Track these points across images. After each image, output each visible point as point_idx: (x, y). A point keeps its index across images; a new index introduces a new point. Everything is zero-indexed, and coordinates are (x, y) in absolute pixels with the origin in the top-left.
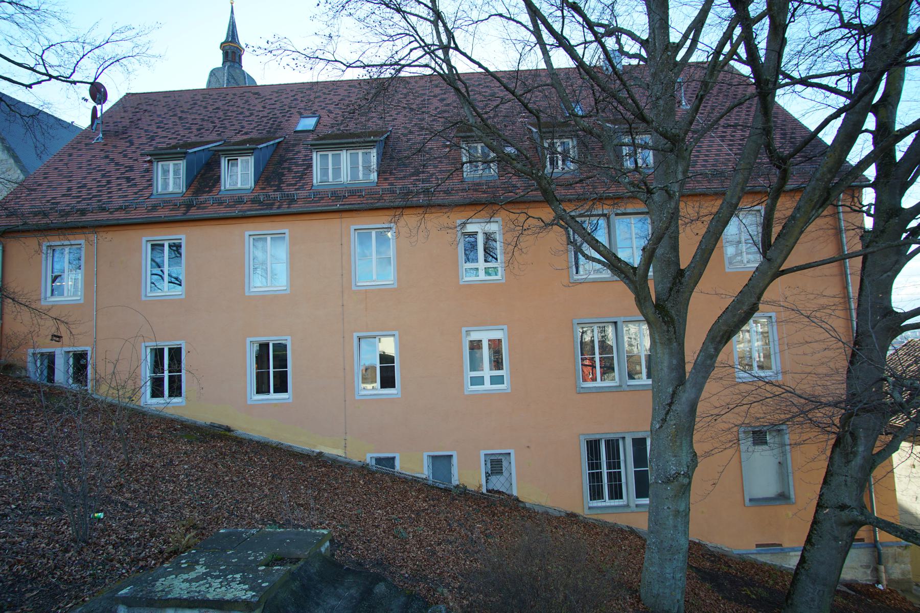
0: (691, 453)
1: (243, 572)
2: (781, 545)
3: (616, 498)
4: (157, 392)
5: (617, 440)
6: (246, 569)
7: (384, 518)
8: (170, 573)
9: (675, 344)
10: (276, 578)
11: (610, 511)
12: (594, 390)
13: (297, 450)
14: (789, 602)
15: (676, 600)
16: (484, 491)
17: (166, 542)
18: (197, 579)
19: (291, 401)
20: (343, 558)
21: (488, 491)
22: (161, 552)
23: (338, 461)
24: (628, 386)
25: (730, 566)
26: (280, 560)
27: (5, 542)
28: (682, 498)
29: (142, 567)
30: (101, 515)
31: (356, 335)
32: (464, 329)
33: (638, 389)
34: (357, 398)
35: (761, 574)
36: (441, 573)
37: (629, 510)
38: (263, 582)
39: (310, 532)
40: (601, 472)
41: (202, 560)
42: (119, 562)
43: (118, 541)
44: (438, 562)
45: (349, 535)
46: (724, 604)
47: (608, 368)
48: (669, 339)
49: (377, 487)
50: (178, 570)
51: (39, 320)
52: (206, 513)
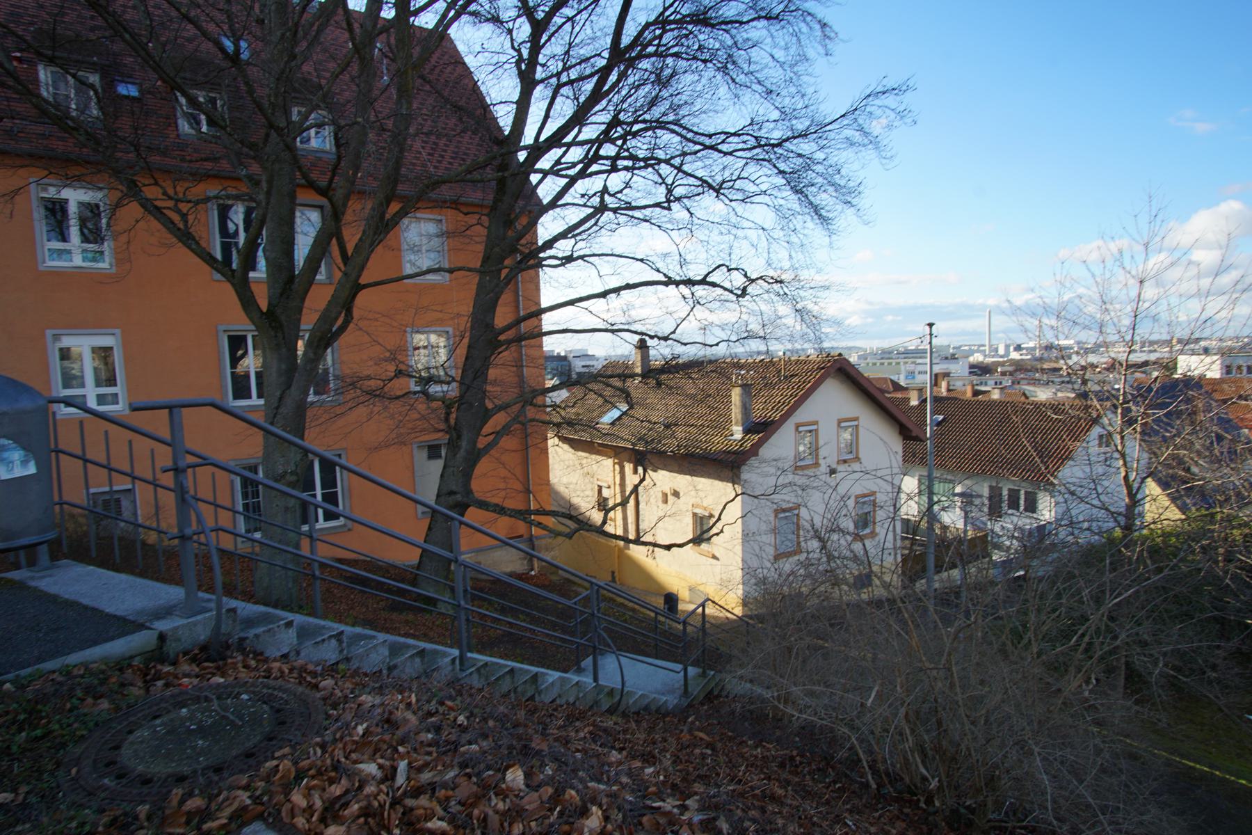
9: (284, 350)
32: (49, 333)
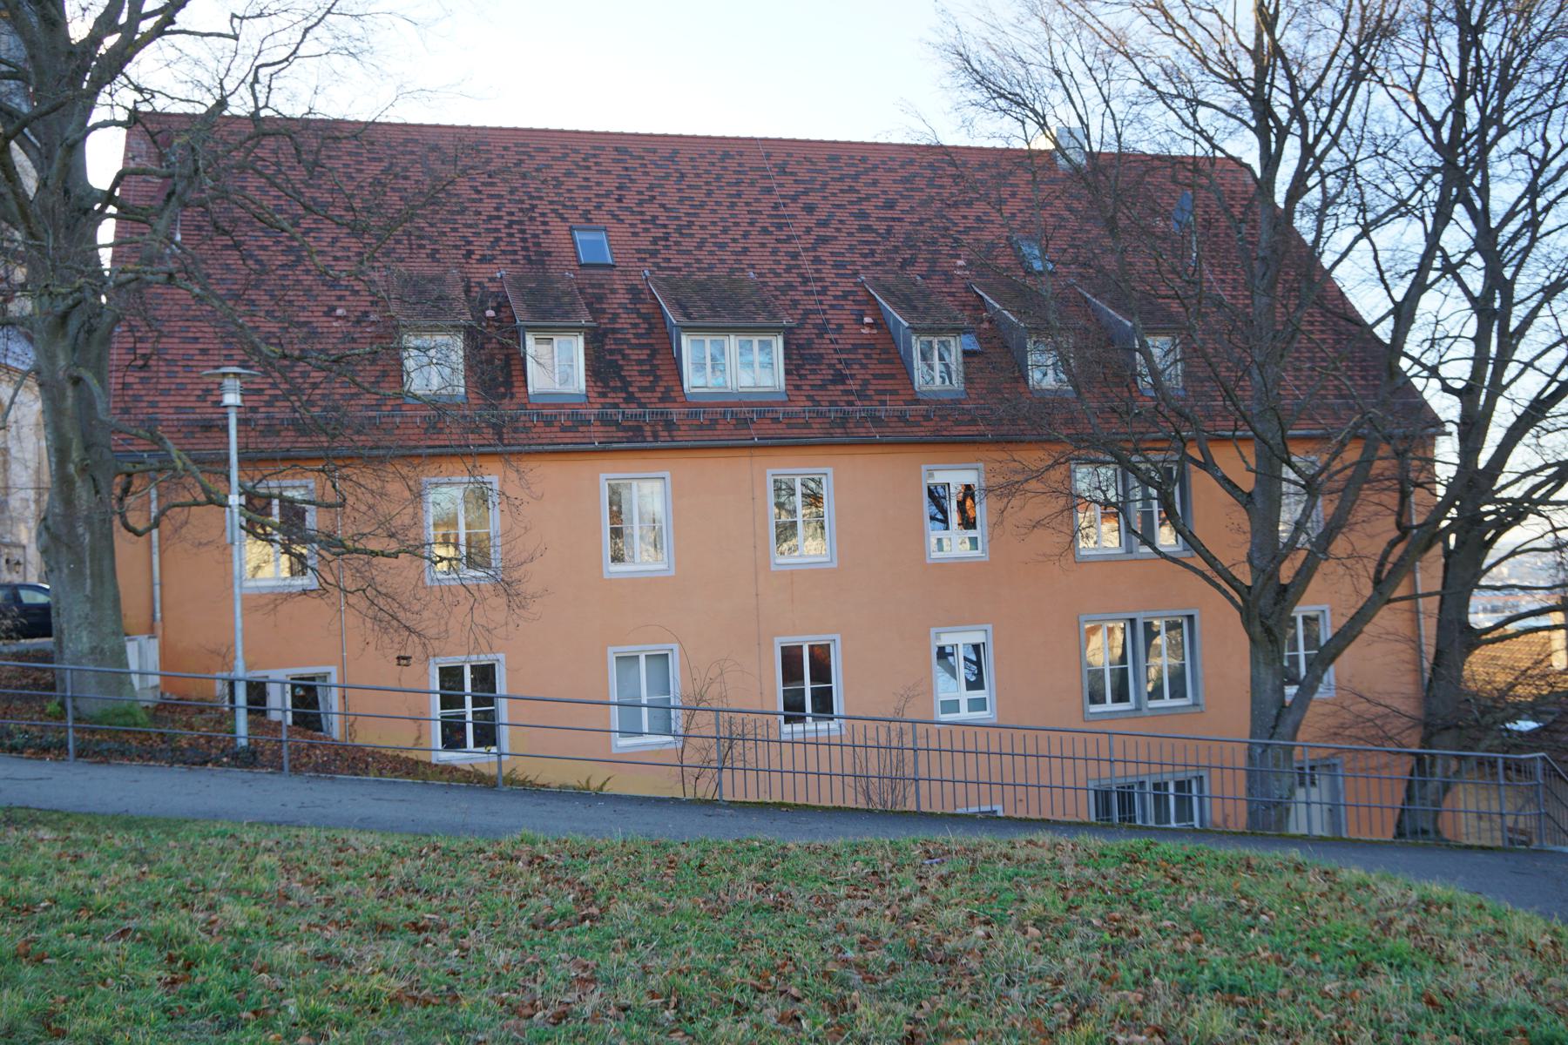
12: (1165, 712)
32: (933, 630)
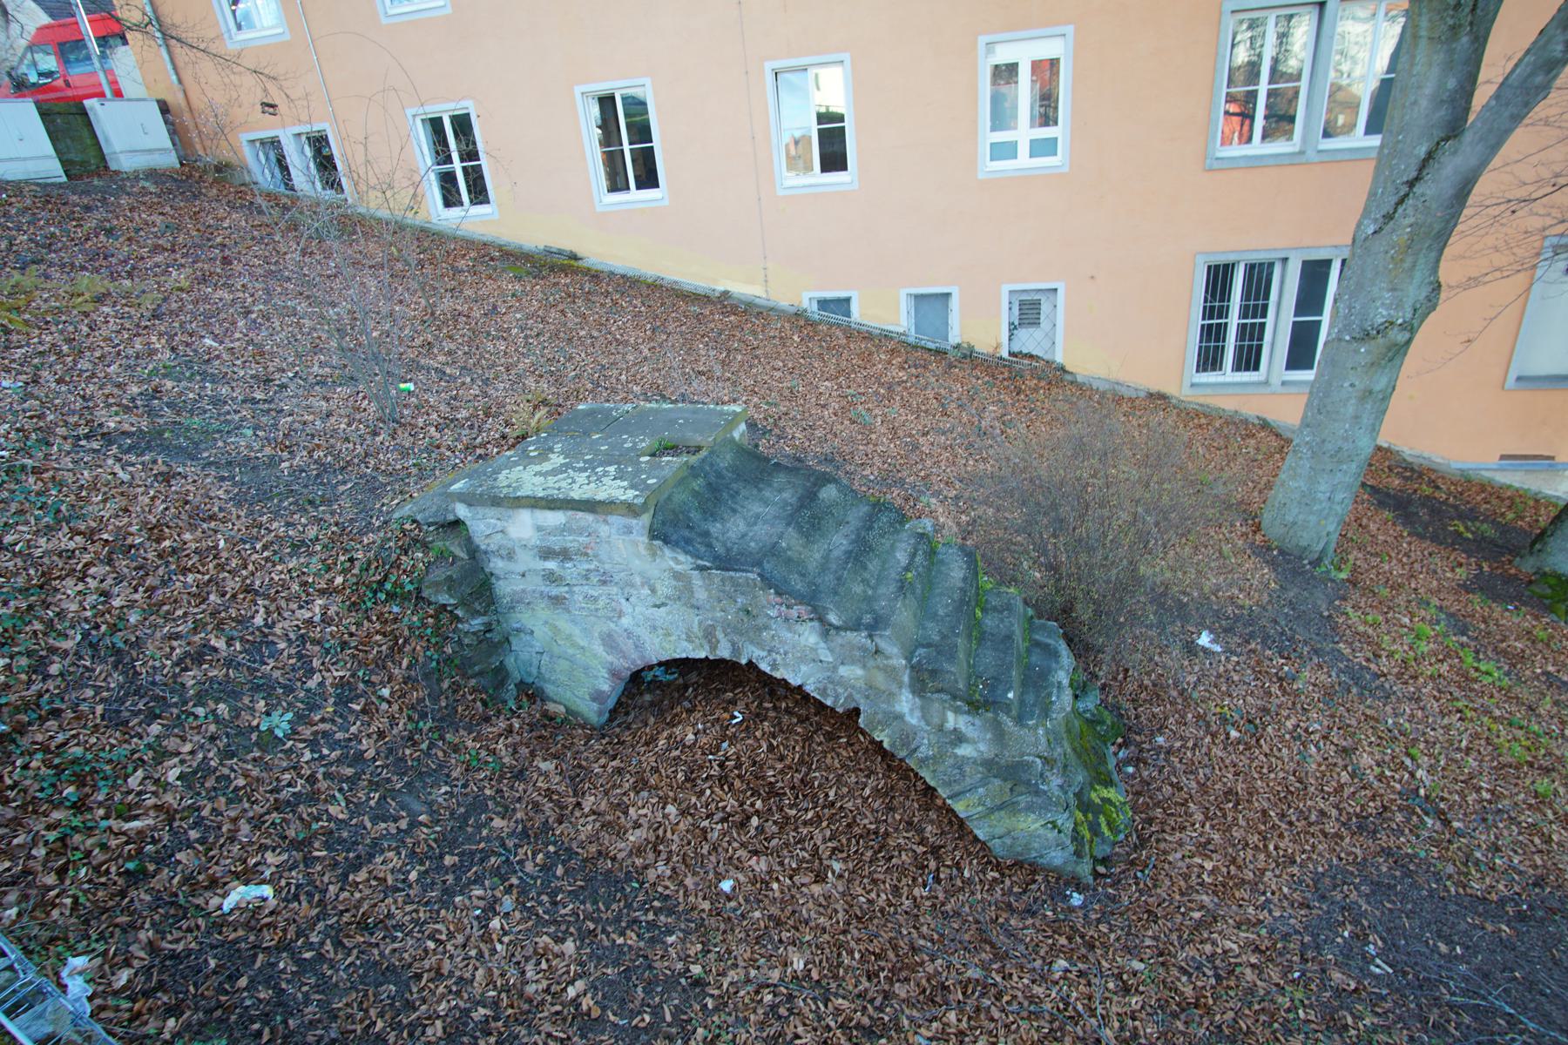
0: (1431, 283)
1: (619, 463)
2: (1552, 458)
3: (1247, 369)
4: (451, 199)
5: (1271, 265)
6: (618, 458)
7: (834, 393)
8: (516, 464)
9: (1465, 40)
10: (667, 472)
11: (1230, 391)
13: (687, 288)
14: (1538, 546)
15: (1324, 533)
16: (1005, 355)
17: (508, 424)
18: (554, 472)
19: (666, 203)
20: (772, 451)
21: (1010, 354)
22: (504, 437)
23: (756, 306)
24: (1320, 151)
25: (1438, 488)
26: (673, 449)
27: (294, 422)
28: (1385, 367)
29: (480, 456)
30: (410, 386)
31: (769, 66)
32: (983, 40)
33: (1339, 157)
34: (780, 193)
35: (1494, 501)
36: (927, 476)
37: (1268, 390)
38: (648, 478)
39: (714, 410)
40: (1226, 324)
41: (558, 448)
42: (449, 448)
43: (441, 421)
44: (922, 460)
45: (780, 418)
46: (1410, 544)
47: (1281, 120)
48: (1453, 28)
49: (821, 346)
50: (527, 460)
51: (232, 77)
52: (558, 382)
